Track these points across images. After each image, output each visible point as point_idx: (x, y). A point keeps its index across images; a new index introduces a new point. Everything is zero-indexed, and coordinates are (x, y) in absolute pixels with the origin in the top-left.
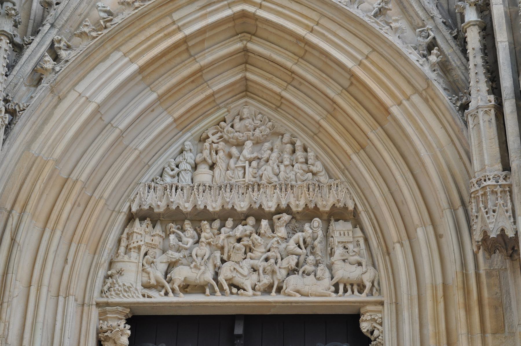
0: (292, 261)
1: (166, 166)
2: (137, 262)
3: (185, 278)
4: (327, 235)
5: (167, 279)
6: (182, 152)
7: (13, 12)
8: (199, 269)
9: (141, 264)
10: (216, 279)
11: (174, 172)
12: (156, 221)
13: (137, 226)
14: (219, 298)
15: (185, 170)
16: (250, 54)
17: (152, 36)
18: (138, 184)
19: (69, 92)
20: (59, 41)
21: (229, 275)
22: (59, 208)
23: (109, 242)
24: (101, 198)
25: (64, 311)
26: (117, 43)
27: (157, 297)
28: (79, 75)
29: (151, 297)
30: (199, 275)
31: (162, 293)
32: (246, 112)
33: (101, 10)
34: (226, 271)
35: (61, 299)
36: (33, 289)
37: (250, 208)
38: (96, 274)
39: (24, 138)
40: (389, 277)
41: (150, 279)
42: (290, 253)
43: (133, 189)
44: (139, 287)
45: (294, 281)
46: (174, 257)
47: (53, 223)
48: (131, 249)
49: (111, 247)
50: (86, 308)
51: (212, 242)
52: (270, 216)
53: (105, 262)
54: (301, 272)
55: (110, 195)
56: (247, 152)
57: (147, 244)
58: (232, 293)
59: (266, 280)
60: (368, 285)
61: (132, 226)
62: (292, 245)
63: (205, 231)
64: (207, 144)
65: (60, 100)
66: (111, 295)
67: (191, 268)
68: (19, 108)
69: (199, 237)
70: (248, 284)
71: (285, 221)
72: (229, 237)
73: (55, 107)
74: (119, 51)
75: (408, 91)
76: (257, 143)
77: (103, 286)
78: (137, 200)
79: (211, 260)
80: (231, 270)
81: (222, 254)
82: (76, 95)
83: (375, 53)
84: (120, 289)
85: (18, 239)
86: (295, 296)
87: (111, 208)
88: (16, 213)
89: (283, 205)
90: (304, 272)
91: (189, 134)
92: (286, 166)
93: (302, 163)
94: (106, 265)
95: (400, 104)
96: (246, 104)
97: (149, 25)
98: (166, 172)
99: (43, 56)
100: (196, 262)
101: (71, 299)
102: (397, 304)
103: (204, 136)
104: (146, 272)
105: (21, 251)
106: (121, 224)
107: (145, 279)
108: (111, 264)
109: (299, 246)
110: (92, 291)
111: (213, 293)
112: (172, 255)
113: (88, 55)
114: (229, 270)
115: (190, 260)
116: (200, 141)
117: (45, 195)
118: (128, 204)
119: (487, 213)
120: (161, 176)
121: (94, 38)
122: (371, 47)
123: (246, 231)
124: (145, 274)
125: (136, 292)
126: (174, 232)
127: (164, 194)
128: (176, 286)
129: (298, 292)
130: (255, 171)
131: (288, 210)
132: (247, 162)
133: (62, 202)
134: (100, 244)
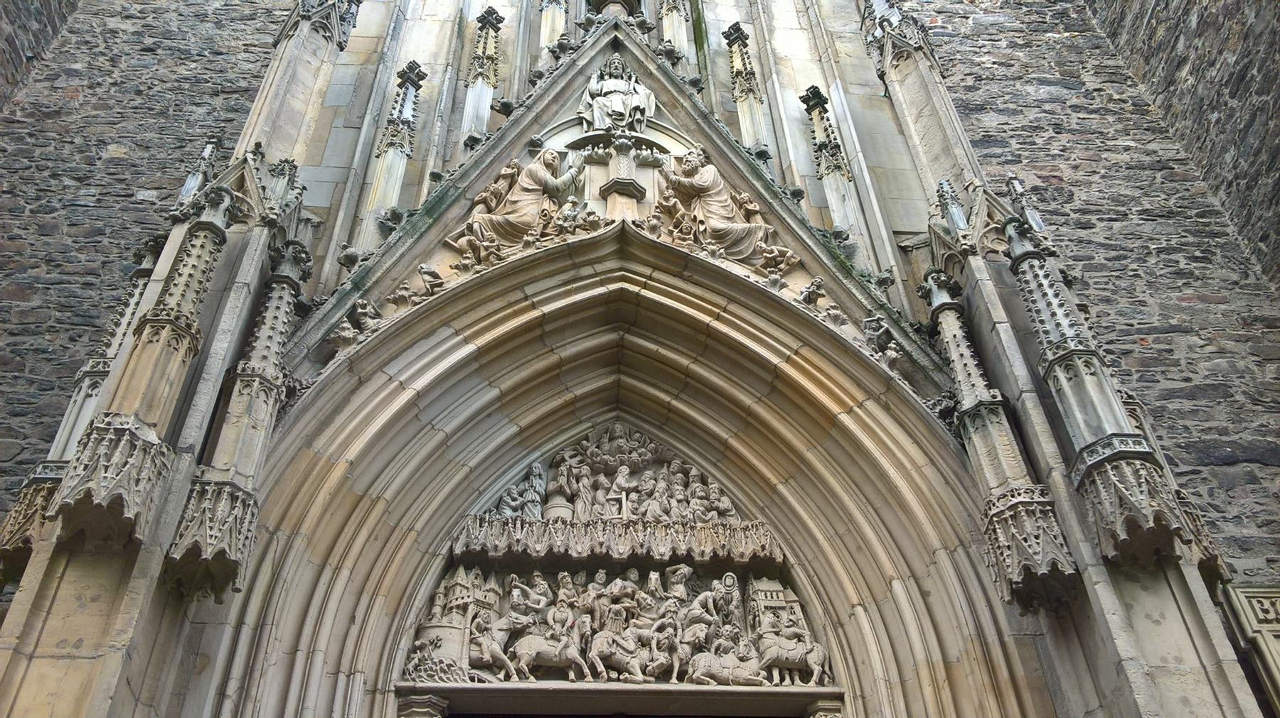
0: (700, 631)
1: (505, 495)
2: (461, 627)
3: (538, 654)
4: (745, 599)
6: (526, 477)
7: (304, 255)
8: (559, 641)
9: (468, 631)
10: (583, 652)
11: (518, 503)
12: (490, 572)
13: (461, 576)
14: (589, 684)
15: (533, 501)
16: (626, 352)
17: (496, 312)
18: (463, 516)
19: (374, 373)
20: (364, 306)
21: (606, 650)
22: (348, 537)
23: (419, 597)
24: (410, 529)
25: (345, 698)
26: (446, 315)
27: (494, 682)
28: (391, 351)
29: (484, 682)
30: (559, 649)
31: (501, 675)
32: (619, 428)
33: (425, 273)
34: (600, 644)
35: (342, 678)
36: (300, 658)
37: (633, 556)
38: (396, 644)
39: (304, 428)
40: (846, 659)
41: (482, 654)
42: (697, 620)
43: (456, 523)
44: (465, 665)
45: (704, 661)
47: (337, 558)
48: (451, 608)
49: (421, 606)
50: (379, 697)
52: (661, 566)
53: (411, 627)
54: (713, 650)
55: (423, 528)
56: (622, 479)
57: (477, 602)
58: (610, 679)
59: (662, 658)
60: (817, 670)
61: (452, 577)
62: (696, 608)
64: (563, 468)
65: (361, 383)
66: (420, 677)
67: (546, 639)
68: (301, 385)
69: (555, 594)
70: (635, 664)
71: (685, 576)
72: (599, 596)
73: (353, 392)
74: (450, 327)
75: (860, 396)
76: (635, 471)
77: (406, 665)
78: (463, 539)
79: (576, 629)
81: (593, 620)
82: (386, 378)
83: (807, 348)
84: (434, 667)
85: (284, 574)
86: (708, 684)
87: (423, 548)
88: (282, 536)
89: (682, 549)
90: (717, 649)
91: (538, 454)
92: (679, 501)
93: (701, 498)
94: (412, 631)
95: (850, 411)
96: (618, 418)
97: (491, 299)
98: (505, 502)
99: (340, 321)
101: (359, 678)
102: (863, 698)
103: (558, 458)
104: (476, 644)
105: (287, 592)
106: (435, 577)
107: (475, 654)
108: (418, 633)
109: (707, 611)
110: (389, 669)
111: (581, 676)
113: (403, 327)
114: (605, 644)
115: (544, 628)
116: (551, 466)
117: (328, 516)
118: (449, 543)
119: (1025, 540)
120: (497, 507)
121: (416, 304)
122: (801, 341)
123: (625, 588)
124: (474, 647)
125: (460, 673)
126: (516, 587)
127: (504, 530)
128: (523, 665)
129: (712, 677)
130: (636, 505)
131: (688, 559)
132: (624, 493)
133: (353, 528)
134: (405, 599)
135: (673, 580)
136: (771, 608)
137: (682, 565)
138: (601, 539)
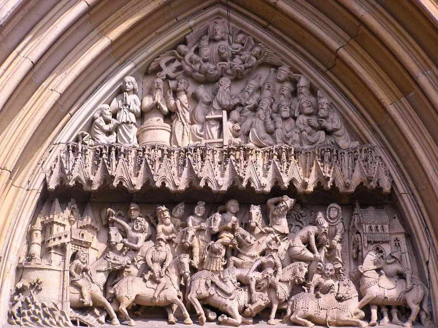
5: (108, 297)
46: (117, 262)
51: (174, 239)
54: (312, 289)
58: (209, 320)
63: (163, 223)
80: (206, 284)
90: (317, 288)
100: (152, 271)
112: (114, 259)
136: (375, 242)
137: (286, 197)
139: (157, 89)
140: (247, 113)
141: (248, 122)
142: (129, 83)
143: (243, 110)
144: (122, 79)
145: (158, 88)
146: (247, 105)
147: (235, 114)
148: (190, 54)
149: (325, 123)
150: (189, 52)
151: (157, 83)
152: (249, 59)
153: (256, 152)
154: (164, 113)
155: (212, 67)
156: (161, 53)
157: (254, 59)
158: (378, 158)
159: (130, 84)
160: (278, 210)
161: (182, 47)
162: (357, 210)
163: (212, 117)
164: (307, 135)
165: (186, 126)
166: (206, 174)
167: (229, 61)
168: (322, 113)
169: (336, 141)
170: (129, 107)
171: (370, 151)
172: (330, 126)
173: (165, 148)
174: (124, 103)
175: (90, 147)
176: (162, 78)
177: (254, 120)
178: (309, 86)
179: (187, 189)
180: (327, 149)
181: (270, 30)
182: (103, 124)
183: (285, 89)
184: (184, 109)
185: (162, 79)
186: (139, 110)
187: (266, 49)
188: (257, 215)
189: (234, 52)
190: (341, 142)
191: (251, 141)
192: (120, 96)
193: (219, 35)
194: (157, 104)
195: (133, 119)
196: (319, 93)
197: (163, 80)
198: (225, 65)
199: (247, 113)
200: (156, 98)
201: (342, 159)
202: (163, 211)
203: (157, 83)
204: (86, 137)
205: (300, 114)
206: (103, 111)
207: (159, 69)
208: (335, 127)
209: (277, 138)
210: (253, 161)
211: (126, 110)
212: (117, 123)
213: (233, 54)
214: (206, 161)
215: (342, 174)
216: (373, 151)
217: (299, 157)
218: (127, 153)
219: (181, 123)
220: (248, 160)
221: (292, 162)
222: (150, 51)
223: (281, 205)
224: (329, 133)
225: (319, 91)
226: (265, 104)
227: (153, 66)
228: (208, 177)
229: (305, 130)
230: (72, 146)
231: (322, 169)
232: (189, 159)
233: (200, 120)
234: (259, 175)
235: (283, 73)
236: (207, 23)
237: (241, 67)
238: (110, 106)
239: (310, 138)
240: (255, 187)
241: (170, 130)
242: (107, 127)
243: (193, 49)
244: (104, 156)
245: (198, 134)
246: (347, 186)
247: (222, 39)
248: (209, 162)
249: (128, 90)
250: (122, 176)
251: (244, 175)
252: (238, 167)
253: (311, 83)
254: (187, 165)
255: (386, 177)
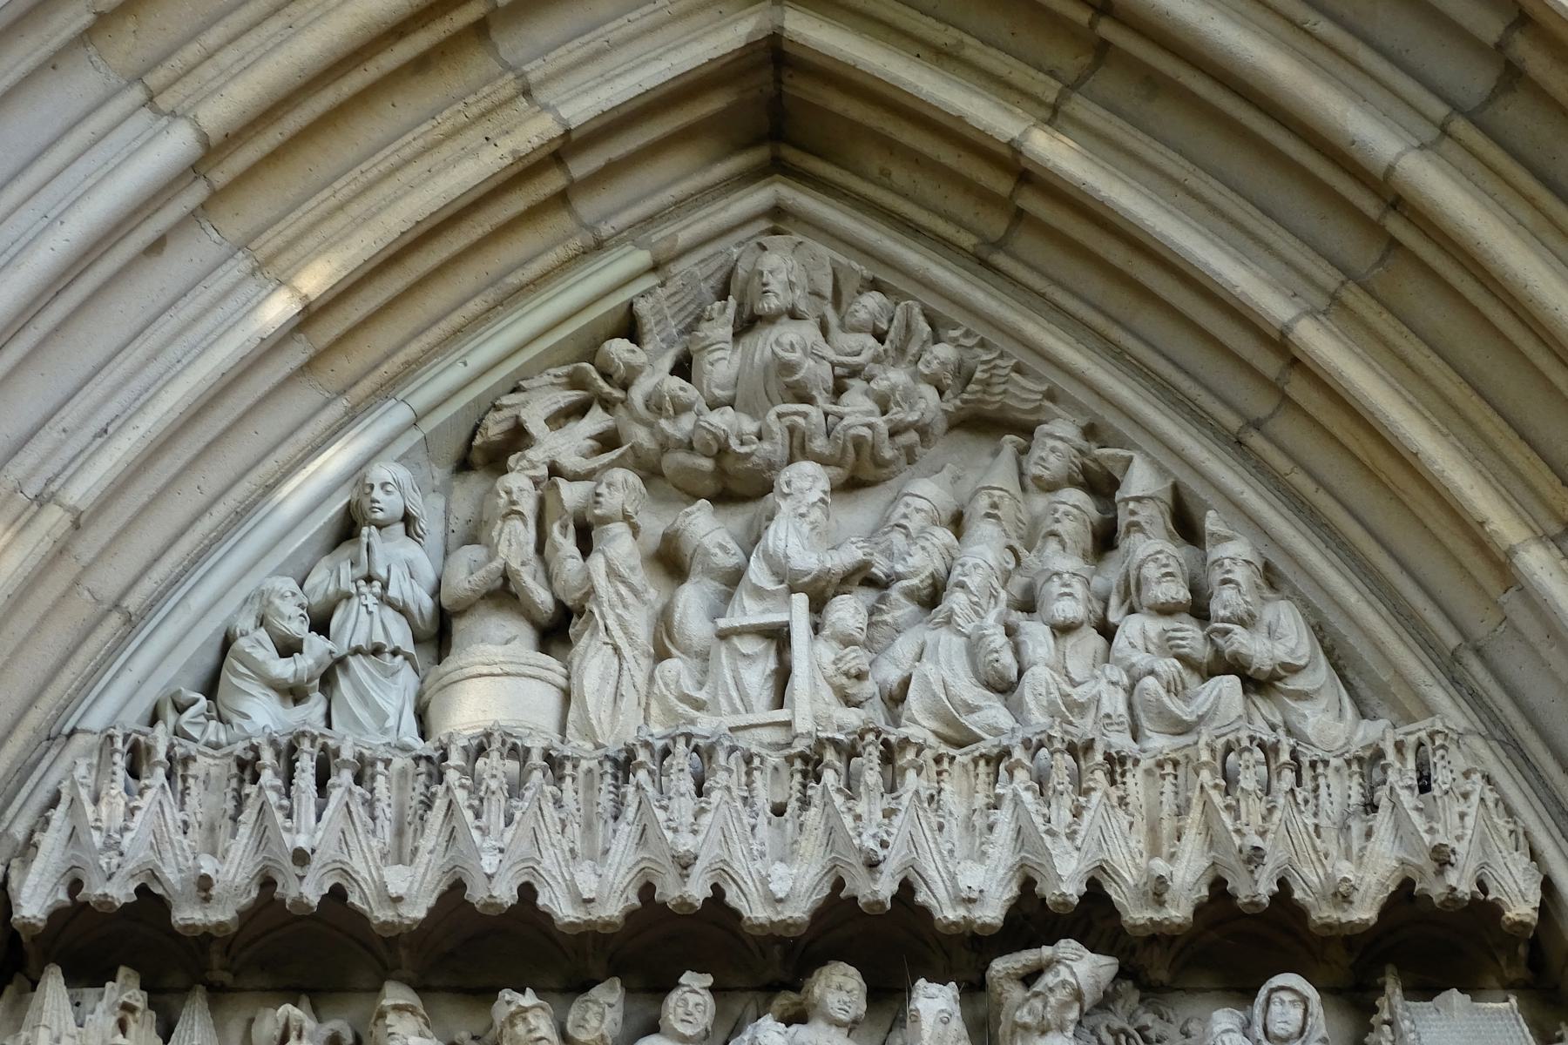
135: (1023, 1016)
137: (1068, 948)
138: (686, 843)
139: (505, 517)
140: (901, 609)
141: (904, 647)
142: (384, 485)
143: (882, 600)
144: (357, 475)
145: (513, 513)
146: (900, 577)
147: (848, 611)
148: (656, 377)
149: (1242, 641)
150: (648, 369)
151: (509, 493)
152: (909, 398)
153: (938, 760)
154: (538, 617)
155: (749, 426)
156: (526, 372)
157: (930, 393)
158: (1477, 777)
159: (388, 493)
160: (1037, 1004)
161: (619, 349)
162: (1393, 998)
163: (746, 621)
164: (1162, 692)
165: (629, 663)
166: (717, 851)
167: (820, 400)
168: (1225, 602)
169: (1294, 718)
170: (385, 587)
171: (1443, 747)
172: (1258, 649)
173: (536, 745)
174: (363, 570)
175: (210, 751)
176: (532, 473)
177: (929, 636)
178: (1168, 498)
179: (630, 915)
180: (1252, 739)
181: (996, 270)
182: (266, 654)
183: (1067, 514)
184: (623, 590)
185: (531, 478)
186: (428, 604)
187: (979, 351)
188: (946, 1022)
189: (842, 365)
190: (1311, 720)
191: (919, 718)
192: (346, 550)
193: (777, 295)
194: (506, 576)
195: (400, 635)
196: (1212, 522)
197: (536, 483)
198: (805, 415)
199: (898, 613)
200: (503, 549)
201: (1316, 789)
202: (526, 1010)
203: (509, 493)
204: (192, 711)
205: (1132, 611)
206: (270, 603)
207: (518, 437)
208: (1288, 660)
209: (1032, 704)
210: (925, 795)
211: (371, 600)
212: (331, 652)
213: (837, 378)
214: (715, 797)
215: (1318, 842)
216: (1453, 748)
217: (1129, 778)
218: (368, 771)
219: (609, 649)
220: (901, 791)
221: (1096, 797)
222: (482, 355)
223: (1049, 979)
224: (1257, 684)
225: (1211, 513)
226: (976, 566)
227: (495, 428)
228: (724, 861)
229: (1152, 672)
230: (126, 737)
231: (1226, 818)
232: (638, 787)
233: (695, 641)
234: (951, 852)
235: (1053, 450)
236: (730, 247)
237: (870, 426)
238: (301, 587)
239: (1175, 706)
240: (933, 902)
241: (562, 681)
242: (284, 669)
243: (667, 362)
244: (267, 777)
245: (685, 698)
246: (1343, 898)
247: (794, 315)
248: (727, 798)
249: (380, 515)
250: (346, 859)
251: (884, 845)
252: (858, 818)
253: (1176, 489)
254: (630, 813)
255: (1516, 855)
